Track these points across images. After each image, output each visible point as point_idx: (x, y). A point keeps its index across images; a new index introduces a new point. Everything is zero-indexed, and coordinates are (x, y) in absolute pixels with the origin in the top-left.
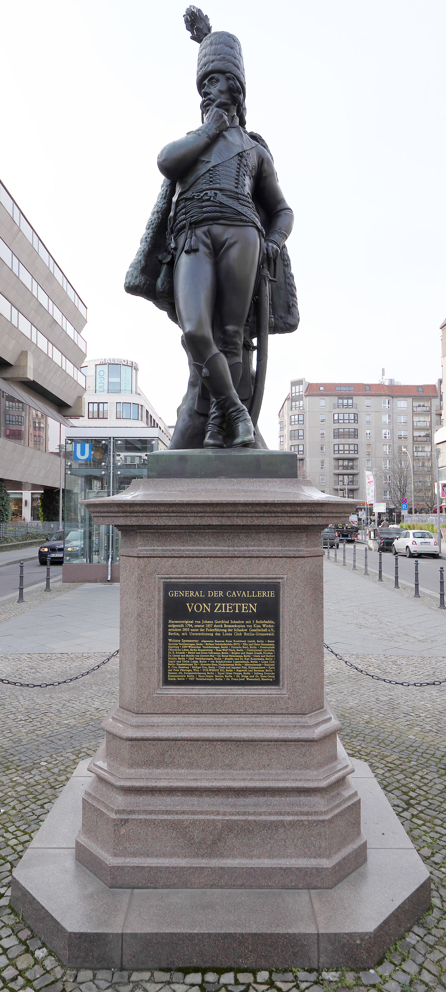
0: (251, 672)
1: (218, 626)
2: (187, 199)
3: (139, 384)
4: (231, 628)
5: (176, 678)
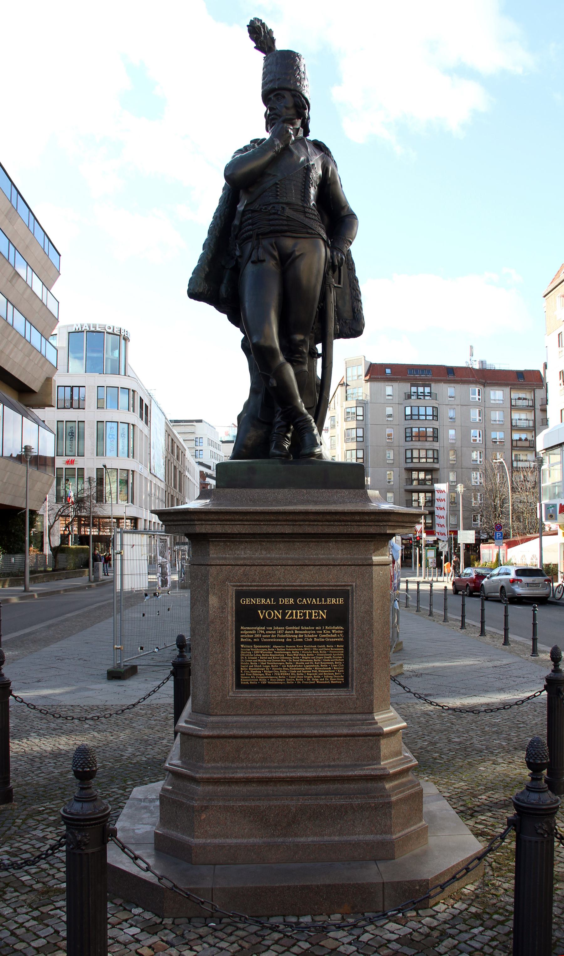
0: (321, 676)
1: (289, 632)
2: (253, 211)
3: (129, 361)
4: (301, 634)
5: (249, 682)
